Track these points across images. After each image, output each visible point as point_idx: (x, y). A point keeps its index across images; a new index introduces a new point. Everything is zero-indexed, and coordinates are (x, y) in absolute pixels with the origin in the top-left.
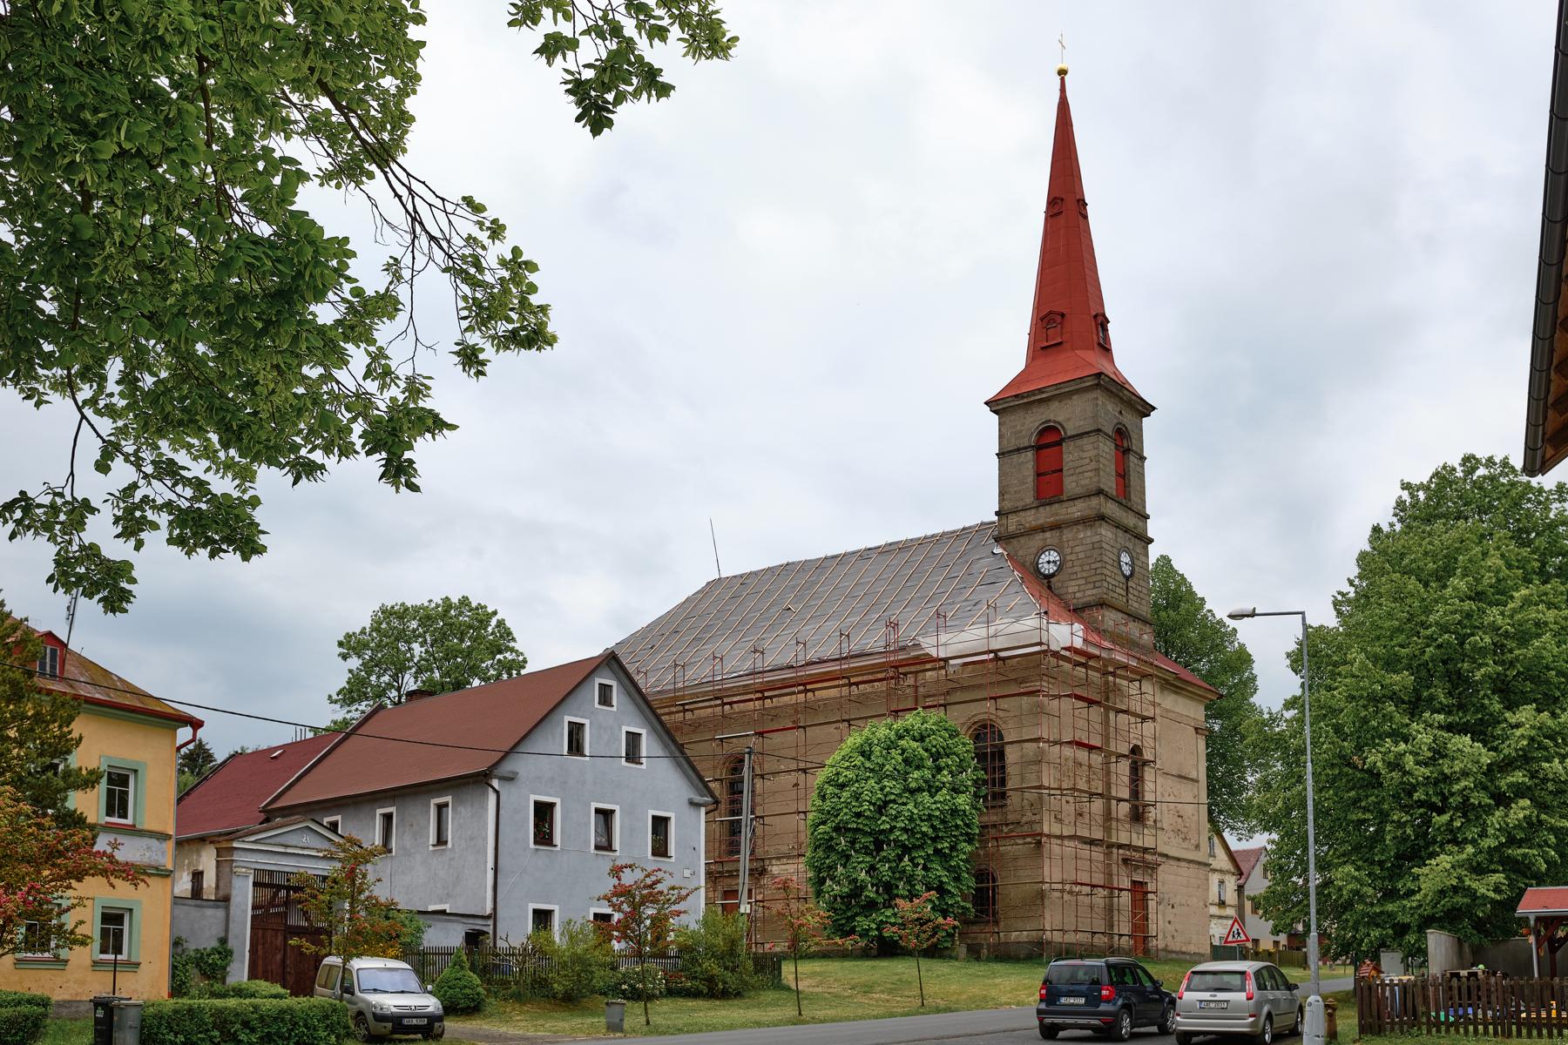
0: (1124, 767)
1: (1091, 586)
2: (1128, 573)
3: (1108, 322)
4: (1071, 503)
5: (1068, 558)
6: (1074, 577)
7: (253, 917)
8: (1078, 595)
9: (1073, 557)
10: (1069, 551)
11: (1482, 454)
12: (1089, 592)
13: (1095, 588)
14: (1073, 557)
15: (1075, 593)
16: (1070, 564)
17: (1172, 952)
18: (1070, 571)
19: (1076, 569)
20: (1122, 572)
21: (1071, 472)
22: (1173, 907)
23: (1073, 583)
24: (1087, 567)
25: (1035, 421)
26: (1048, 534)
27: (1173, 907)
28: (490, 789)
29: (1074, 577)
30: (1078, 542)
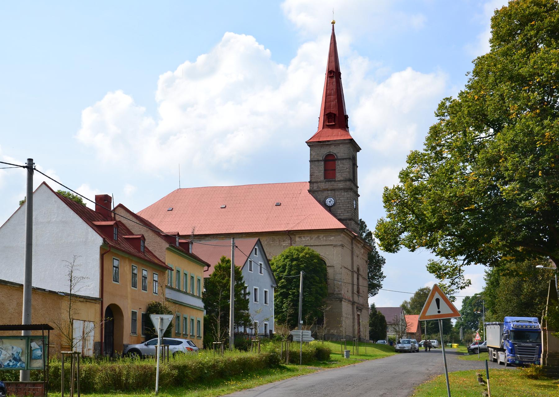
5: (338, 201)
6: (340, 208)
8: (341, 215)
9: (340, 201)
10: (338, 199)
13: (348, 213)
14: (340, 201)
18: (338, 206)
21: (339, 171)
23: (339, 210)
26: (329, 192)
29: (340, 208)
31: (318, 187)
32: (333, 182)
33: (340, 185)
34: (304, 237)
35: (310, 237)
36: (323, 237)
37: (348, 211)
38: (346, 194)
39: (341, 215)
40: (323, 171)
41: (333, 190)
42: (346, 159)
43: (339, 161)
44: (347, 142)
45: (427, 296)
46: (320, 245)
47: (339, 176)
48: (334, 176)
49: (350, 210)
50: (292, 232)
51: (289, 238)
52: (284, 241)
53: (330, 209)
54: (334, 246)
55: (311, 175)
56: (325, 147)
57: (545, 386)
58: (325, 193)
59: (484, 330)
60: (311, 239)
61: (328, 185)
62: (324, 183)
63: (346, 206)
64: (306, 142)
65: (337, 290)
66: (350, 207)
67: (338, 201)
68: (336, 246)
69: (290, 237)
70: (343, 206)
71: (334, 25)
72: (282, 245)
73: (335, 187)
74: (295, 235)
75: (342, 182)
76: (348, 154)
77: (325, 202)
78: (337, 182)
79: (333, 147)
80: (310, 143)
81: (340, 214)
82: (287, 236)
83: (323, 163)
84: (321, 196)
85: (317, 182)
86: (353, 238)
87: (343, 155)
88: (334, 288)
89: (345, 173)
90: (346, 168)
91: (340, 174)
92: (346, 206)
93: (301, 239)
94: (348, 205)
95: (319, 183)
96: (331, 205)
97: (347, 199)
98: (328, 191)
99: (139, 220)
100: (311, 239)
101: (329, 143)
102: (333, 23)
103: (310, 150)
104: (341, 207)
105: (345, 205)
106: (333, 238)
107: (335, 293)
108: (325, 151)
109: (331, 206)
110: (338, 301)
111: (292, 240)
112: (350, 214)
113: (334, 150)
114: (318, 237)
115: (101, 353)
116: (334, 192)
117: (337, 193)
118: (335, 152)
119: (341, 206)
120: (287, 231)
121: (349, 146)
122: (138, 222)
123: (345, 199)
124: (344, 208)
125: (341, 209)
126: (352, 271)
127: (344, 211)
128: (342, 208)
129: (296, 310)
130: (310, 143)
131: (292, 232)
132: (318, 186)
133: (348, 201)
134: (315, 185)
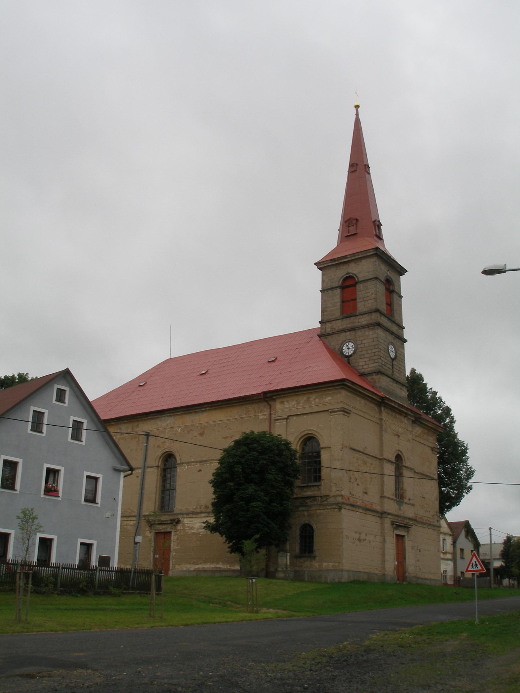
0: (390, 469)
2: (393, 357)
3: (382, 225)
4: (361, 317)
6: (363, 357)
8: (365, 367)
9: (362, 346)
10: (360, 342)
12: (370, 366)
13: (374, 363)
14: (362, 346)
16: (360, 350)
17: (418, 578)
19: (364, 352)
21: (362, 300)
22: (420, 551)
23: (362, 360)
26: (348, 333)
27: (420, 551)
31: (332, 328)
32: (353, 318)
33: (363, 320)
34: (288, 401)
35: (297, 401)
36: (315, 399)
37: (374, 360)
38: (371, 333)
39: (365, 367)
40: (339, 304)
41: (353, 329)
42: (370, 279)
43: (361, 285)
44: (371, 253)
46: (311, 413)
47: (361, 307)
48: (355, 308)
49: (377, 357)
50: (269, 395)
51: (268, 407)
52: (261, 412)
53: (348, 360)
54: (331, 412)
55: (323, 312)
56: (341, 267)
58: (342, 336)
60: (298, 403)
61: (346, 323)
62: (340, 321)
64: (315, 264)
65: (334, 489)
66: (377, 354)
67: (359, 346)
68: (334, 412)
69: (270, 405)
70: (368, 353)
71: (359, 109)
72: (258, 418)
73: (356, 325)
74: (274, 400)
75: (365, 315)
76: (373, 271)
77: (342, 349)
78: (359, 317)
79: (352, 265)
80: (322, 265)
81: (363, 366)
82: (266, 403)
83: (338, 291)
84: (334, 342)
85: (330, 321)
86: (380, 403)
87: (367, 274)
88: (331, 486)
89: (369, 301)
90: (370, 294)
91: (363, 303)
93: (284, 405)
94: (374, 351)
95: (334, 322)
96: (350, 354)
97: (374, 341)
98: (346, 332)
100: (298, 403)
101: (346, 260)
102: (357, 107)
103: (322, 275)
104: (364, 355)
105: (370, 352)
106: (329, 398)
107: (332, 494)
108: (341, 273)
109: (351, 356)
110: (335, 508)
111: (272, 408)
112: (377, 364)
113: (353, 269)
114: (308, 398)
116: (354, 333)
117: (359, 333)
118: (354, 272)
119: (364, 352)
120: (262, 394)
121: (374, 260)
124: (369, 355)
125: (364, 358)
127: (370, 360)
128: (366, 356)
129: (152, 522)
130: (322, 265)
131: (269, 395)
132: (332, 326)
133: (375, 343)
134: (328, 325)
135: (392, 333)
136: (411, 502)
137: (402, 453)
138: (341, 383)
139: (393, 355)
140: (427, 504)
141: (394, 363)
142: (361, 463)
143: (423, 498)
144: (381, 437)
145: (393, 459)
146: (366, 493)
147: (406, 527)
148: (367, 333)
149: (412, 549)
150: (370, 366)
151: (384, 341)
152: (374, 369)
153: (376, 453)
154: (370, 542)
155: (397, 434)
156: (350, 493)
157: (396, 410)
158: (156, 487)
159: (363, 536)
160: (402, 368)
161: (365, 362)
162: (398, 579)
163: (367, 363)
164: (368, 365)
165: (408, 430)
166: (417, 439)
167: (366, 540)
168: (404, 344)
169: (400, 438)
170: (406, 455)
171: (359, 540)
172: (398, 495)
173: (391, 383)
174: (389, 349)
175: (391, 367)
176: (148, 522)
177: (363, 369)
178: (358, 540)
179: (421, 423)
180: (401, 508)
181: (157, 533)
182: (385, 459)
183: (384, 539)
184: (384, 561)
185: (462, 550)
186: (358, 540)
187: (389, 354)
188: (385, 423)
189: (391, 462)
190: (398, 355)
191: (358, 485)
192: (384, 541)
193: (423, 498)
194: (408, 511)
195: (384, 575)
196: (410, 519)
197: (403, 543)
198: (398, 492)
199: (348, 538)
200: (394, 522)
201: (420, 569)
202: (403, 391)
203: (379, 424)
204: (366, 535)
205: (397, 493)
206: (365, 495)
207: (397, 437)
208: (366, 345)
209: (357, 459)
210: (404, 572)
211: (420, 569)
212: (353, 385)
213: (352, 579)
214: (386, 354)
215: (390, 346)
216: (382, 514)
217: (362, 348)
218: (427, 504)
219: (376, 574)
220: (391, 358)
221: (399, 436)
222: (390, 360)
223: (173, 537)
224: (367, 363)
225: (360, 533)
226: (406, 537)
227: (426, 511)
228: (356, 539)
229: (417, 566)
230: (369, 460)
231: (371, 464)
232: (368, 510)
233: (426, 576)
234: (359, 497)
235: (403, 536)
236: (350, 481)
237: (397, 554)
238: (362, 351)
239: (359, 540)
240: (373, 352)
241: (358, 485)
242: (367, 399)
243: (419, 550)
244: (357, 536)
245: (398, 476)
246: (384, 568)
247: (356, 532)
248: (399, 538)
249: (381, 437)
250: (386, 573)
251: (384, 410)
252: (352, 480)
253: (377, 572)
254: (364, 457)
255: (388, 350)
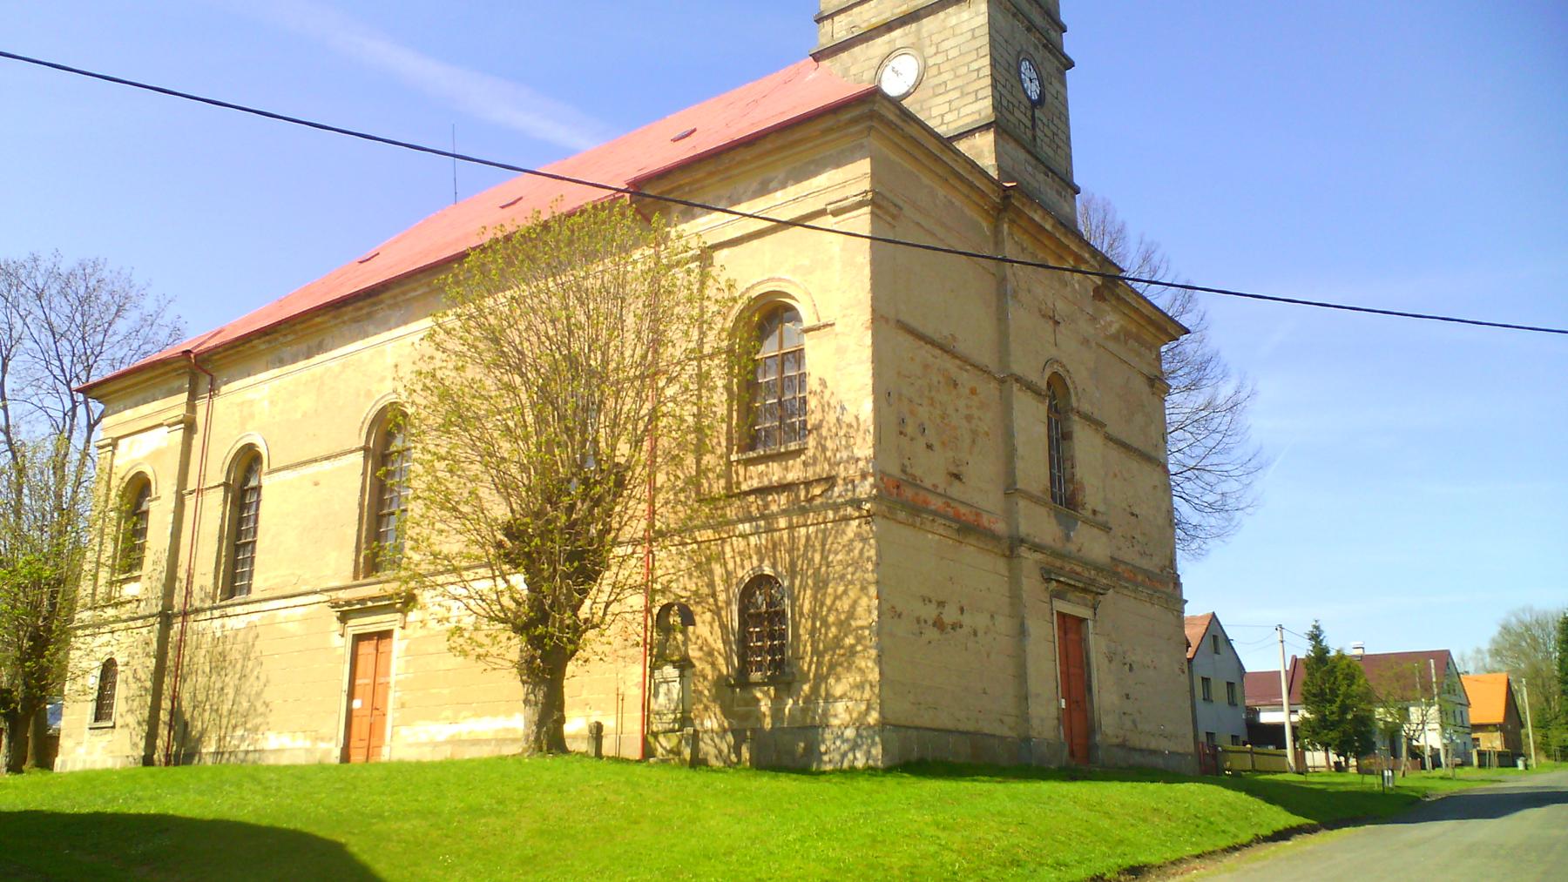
0: (1031, 418)
1: (972, 98)
2: (1035, 97)
5: (931, 62)
6: (942, 89)
7: (1285, 748)
8: (948, 118)
9: (939, 59)
10: (933, 50)
11: (523, 697)
12: (964, 111)
13: (977, 100)
14: (939, 59)
15: (943, 116)
16: (934, 71)
17: (1134, 749)
18: (936, 81)
19: (945, 77)
20: (1025, 91)
22: (1131, 669)
23: (940, 99)
24: (964, 70)
25: (933, 234)
26: (897, 33)
27: (1131, 669)
28: (1230, 754)
30: (947, 33)
38: (965, 15)
45: (1535, 749)
57: (396, 242)
58: (880, 45)
59: (164, 716)
63: (970, 71)
70: (957, 77)
92: (970, 71)
94: (975, 66)
97: (974, 37)
99: (216, 347)
105: (964, 70)
115: (897, 727)
119: (945, 77)
122: (202, 348)
123: (961, 39)
124: (959, 82)
126: (1002, 381)
127: (963, 95)
129: (343, 606)
135: (1031, 27)
136: (1100, 518)
137: (1063, 366)
138: (864, 109)
139: (1033, 90)
140: (1144, 534)
141: (1037, 113)
142: (939, 382)
143: (1133, 514)
144: (1002, 317)
145: (1043, 384)
146: (957, 477)
147: (1090, 591)
148: (953, 21)
149: (1110, 661)
150: (964, 111)
151: (1006, 41)
152: (976, 117)
153: (987, 358)
154: (975, 634)
155: (1051, 315)
156: (904, 471)
157: (1047, 242)
158: (361, 506)
159: (950, 615)
160: (1062, 126)
161: (950, 102)
162: (1072, 754)
163: (955, 105)
164: (958, 109)
165: (1083, 311)
166: (1112, 346)
167: (961, 626)
168: (1065, 74)
169: (1062, 327)
170: (1080, 377)
171: (939, 624)
172: (1059, 477)
173: (1030, 169)
174: (1023, 69)
175: (1029, 124)
176: (332, 607)
177: (942, 123)
178: (934, 624)
179: (1118, 298)
180: (1072, 534)
181: (358, 638)
182: (1018, 380)
183: (1022, 625)
184: (1023, 698)
185: (1206, 681)
186: (934, 624)
187: (1023, 86)
188: (1014, 274)
189: (1037, 392)
190: (1049, 98)
191: (929, 447)
192: (1022, 632)
193: (1133, 514)
194: (1093, 545)
195: (1027, 739)
196: (1099, 569)
197: (1082, 642)
198: (1060, 489)
199: (900, 616)
200: (1049, 572)
201: (1134, 722)
202: (1065, 201)
203: (993, 274)
204: (962, 610)
205: (1056, 490)
206: (957, 483)
207: (1051, 323)
208: (952, 54)
209: (926, 367)
210: (1090, 728)
211: (1134, 722)
212: (904, 121)
213: (915, 756)
214: (1013, 81)
215: (1025, 65)
216: (1012, 546)
217: (939, 64)
218: (1144, 534)
219: (1002, 739)
220: (1029, 98)
221: (1057, 323)
222: (1028, 104)
223: (397, 645)
224: (955, 105)
225: (941, 604)
226: (1090, 623)
227: (1143, 554)
228: (926, 622)
229: (1124, 713)
230: (966, 378)
231: (973, 392)
232: (968, 528)
233: (1153, 744)
234: (935, 486)
235: (1082, 621)
236: (901, 433)
237: (1066, 675)
238: (940, 73)
239: (939, 624)
240: (971, 69)
241: (929, 447)
242: (953, 187)
243: (1127, 667)
244: (930, 612)
245: (1059, 439)
246: (1025, 717)
247: (926, 600)
248: (1070, 627)
249: (1002, 317)
250: (1033, 733)
251: (1011, 234)
252: (910, 429)
253: (1005, 732)
254: (950, 365)
255: (1020, 73)
